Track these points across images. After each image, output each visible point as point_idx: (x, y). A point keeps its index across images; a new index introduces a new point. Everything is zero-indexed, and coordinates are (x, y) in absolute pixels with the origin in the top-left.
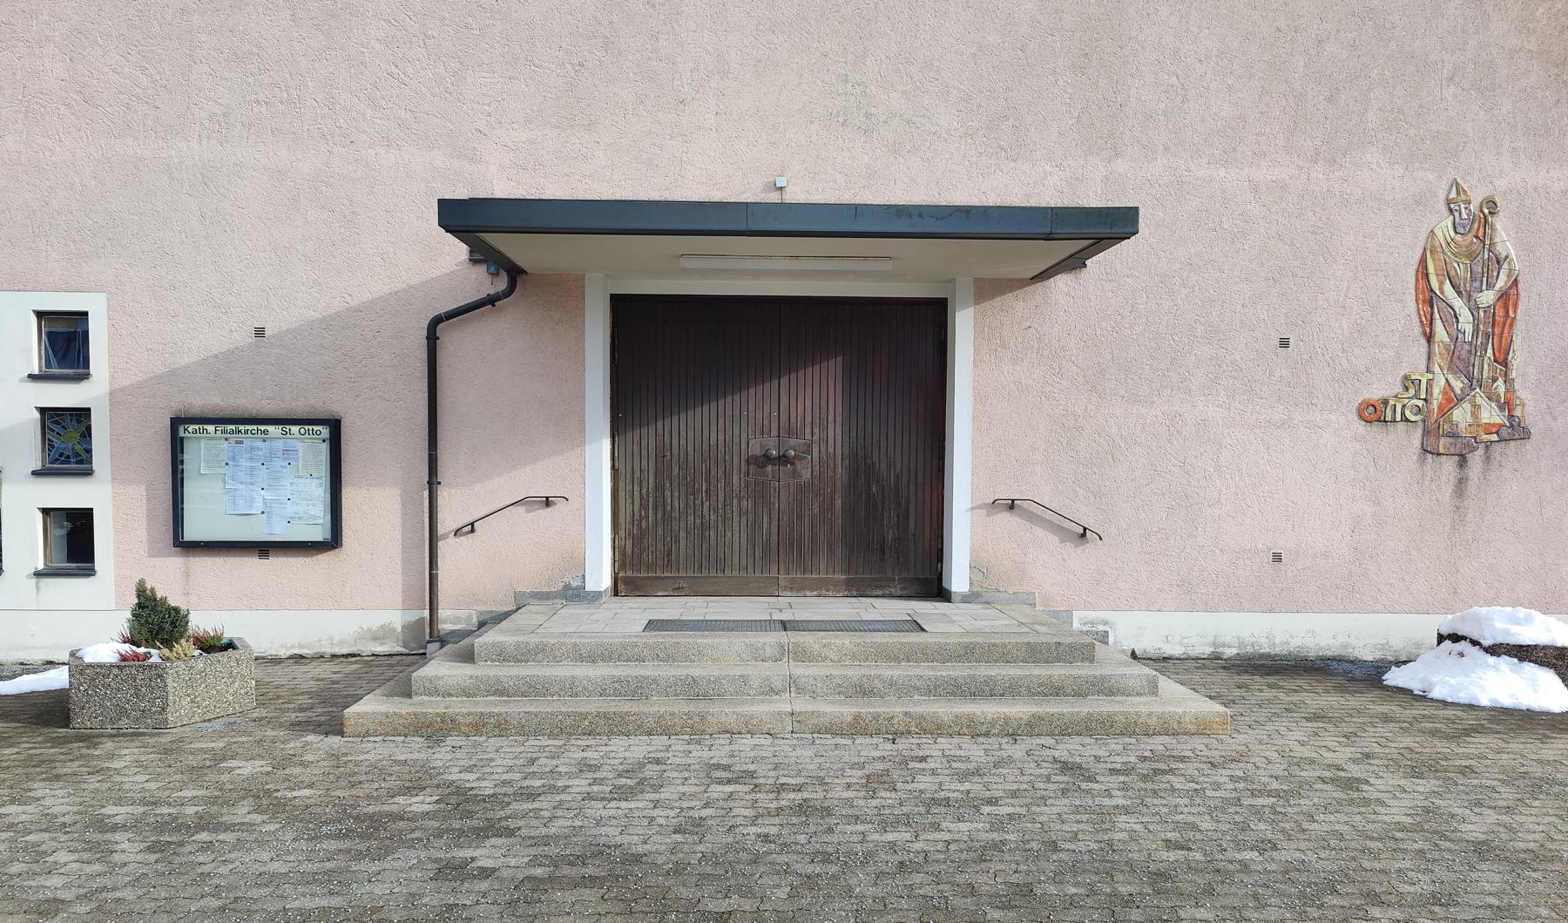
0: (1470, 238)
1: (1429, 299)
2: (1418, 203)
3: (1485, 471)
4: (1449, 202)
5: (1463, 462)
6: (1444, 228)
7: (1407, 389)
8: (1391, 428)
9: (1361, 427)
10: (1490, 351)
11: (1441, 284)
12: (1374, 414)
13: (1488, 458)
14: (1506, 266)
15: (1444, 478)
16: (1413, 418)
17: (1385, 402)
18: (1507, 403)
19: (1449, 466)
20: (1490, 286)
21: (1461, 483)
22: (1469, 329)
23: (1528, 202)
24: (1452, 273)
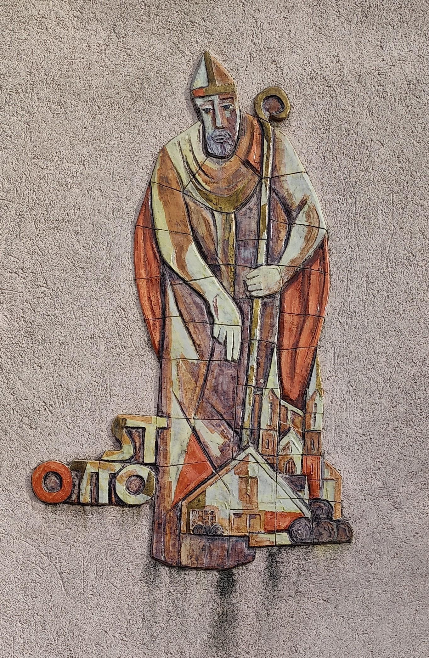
0: (234, 163)
1: (159, 277)
2: (136, 96)
3: (270, 600)
4: (193, 94)
5: (226, 584)
6: (185, 141)
7: (118, 444)
8: (93, 516)
9: (35, 513)
10: (273, 381)
11: (181, 250)
12: (60, 488)
13: (273, 576)
14: (301, 219)
15: (192, 614)
16: (131, 499)
17: (78, 467)
18: (307, 475)
19: (201, 589)
20: (273, 258)
21: (224, 623)
22: (234, 336)
23: (345, 101)
24: (202, 231)
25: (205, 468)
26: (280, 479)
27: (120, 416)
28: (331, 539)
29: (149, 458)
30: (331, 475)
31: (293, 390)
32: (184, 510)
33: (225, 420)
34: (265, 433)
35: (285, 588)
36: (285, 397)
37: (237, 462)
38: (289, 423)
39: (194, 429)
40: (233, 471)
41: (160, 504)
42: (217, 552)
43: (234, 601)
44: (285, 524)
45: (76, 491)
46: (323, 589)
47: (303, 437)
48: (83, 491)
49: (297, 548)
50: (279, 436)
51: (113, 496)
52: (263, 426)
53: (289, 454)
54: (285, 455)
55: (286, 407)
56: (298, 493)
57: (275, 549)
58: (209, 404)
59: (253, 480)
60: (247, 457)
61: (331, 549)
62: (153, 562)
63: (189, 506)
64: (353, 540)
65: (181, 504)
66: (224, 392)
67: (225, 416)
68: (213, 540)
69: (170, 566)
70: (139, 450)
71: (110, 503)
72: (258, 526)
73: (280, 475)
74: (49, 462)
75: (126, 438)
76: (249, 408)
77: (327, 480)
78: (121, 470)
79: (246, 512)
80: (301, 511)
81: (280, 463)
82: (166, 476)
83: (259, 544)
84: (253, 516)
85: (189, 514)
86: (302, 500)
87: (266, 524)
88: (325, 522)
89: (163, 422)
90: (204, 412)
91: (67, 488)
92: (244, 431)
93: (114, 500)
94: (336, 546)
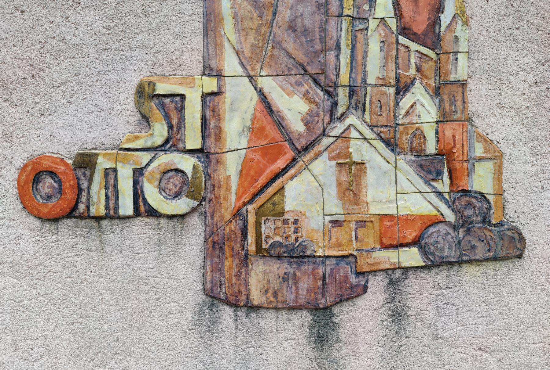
8: (113, 234)
12: (61, 193)
13: (398, 317)
17: (86, 162)
18: (445, 154)
25: (280, 152)
26: (402, 163)
27: (146, 79)
28: (491, 254)
29: (193, 141)
30: (486, 151)
31: (419, 18)
32: (251, 219)
33: (311, 75)
34: (375, 90)
35: (418, 334)
36: (404, 30)
37: (332, 140)
38: (413, 71)
39: (261, 93)
40: (325, 155)
41: (213, 212)
42: (305, 284)
43: (338, 356)
44: (414, 234)
45: (84, 199)
46: (479, 333)
47: (437, 92)
48: (94, 199)
49: (434, 270)
50: (397, 93)
51: (141, 204)
52: (371, 80)
53: (414, 121)
54: (409, 124)
55: (407, 47)
56: (433, 183)
57: (397, 274)
58: (283, 52)
59: (358, 167)
60: (347, 132)
61: (489, 268)
62: (208, 300)
63: (259, 213)
64: (526, 254)
65: (247, 211)
66: (306, 30)
67: (309, 68)
68: (299, 264)
69: (235, 305)
70: (175, 130)
71: (137, 213)
72: (370, 238)
73: (402, 156)
74: (41, 157)
75: (157, 113)
76: (345, 53)
77: (480, 159)
78: (151, 161)
79: (349, 217)
80: (439, 211)
81: (401, 138)
82: (221, 169)
83: (373, 268)
84: (361, 224)
85: (258, 225)
86: (439, 194)
87: (381, 235)
88: (479, 228)
89: (211, 85)
90: (276, 63)
91: (69, 195)
92: (340, 91)
93: (142, 209)
94: (498, 264)
